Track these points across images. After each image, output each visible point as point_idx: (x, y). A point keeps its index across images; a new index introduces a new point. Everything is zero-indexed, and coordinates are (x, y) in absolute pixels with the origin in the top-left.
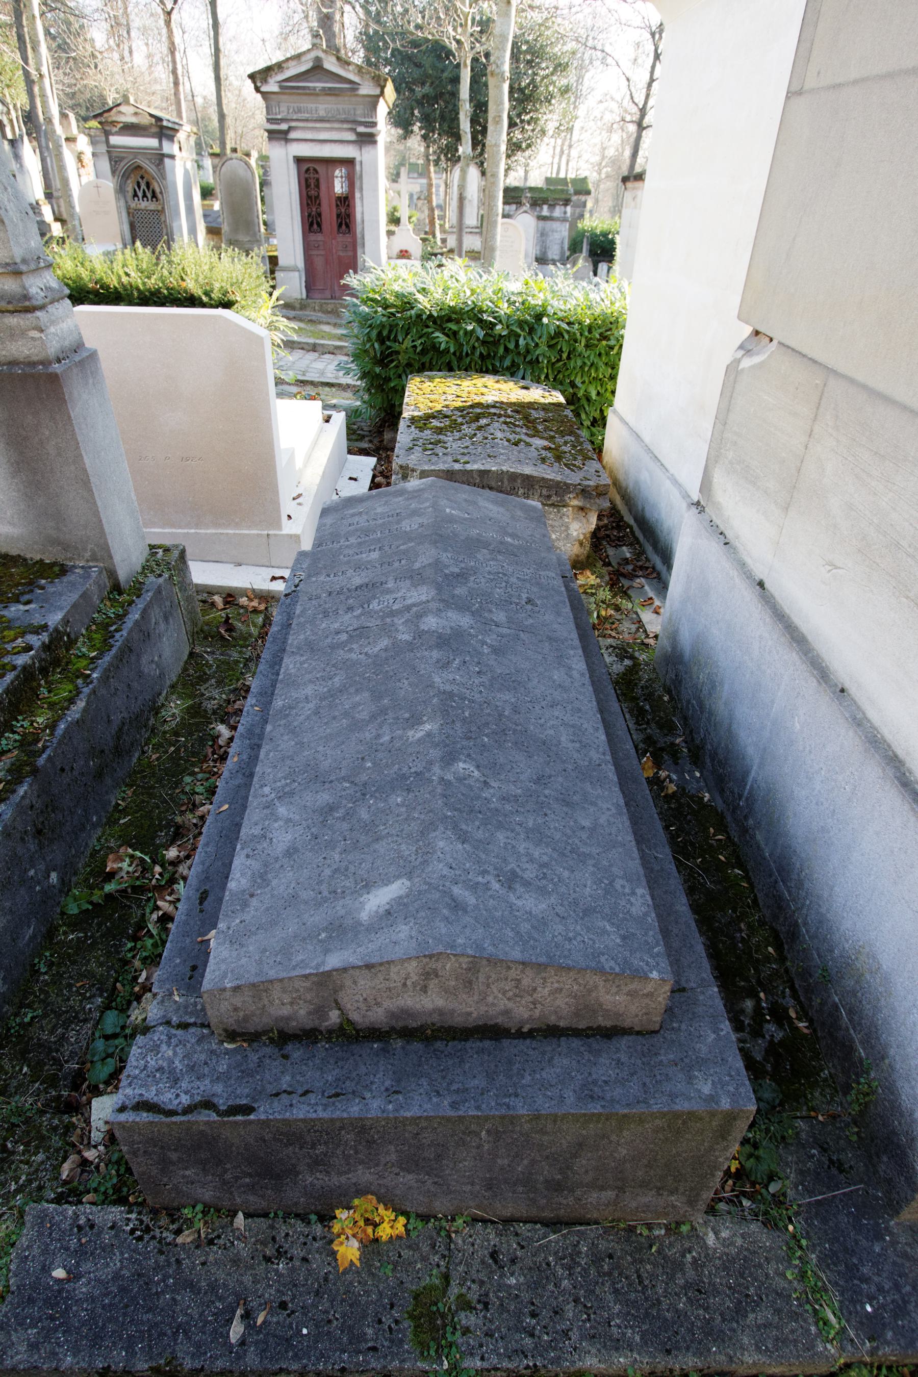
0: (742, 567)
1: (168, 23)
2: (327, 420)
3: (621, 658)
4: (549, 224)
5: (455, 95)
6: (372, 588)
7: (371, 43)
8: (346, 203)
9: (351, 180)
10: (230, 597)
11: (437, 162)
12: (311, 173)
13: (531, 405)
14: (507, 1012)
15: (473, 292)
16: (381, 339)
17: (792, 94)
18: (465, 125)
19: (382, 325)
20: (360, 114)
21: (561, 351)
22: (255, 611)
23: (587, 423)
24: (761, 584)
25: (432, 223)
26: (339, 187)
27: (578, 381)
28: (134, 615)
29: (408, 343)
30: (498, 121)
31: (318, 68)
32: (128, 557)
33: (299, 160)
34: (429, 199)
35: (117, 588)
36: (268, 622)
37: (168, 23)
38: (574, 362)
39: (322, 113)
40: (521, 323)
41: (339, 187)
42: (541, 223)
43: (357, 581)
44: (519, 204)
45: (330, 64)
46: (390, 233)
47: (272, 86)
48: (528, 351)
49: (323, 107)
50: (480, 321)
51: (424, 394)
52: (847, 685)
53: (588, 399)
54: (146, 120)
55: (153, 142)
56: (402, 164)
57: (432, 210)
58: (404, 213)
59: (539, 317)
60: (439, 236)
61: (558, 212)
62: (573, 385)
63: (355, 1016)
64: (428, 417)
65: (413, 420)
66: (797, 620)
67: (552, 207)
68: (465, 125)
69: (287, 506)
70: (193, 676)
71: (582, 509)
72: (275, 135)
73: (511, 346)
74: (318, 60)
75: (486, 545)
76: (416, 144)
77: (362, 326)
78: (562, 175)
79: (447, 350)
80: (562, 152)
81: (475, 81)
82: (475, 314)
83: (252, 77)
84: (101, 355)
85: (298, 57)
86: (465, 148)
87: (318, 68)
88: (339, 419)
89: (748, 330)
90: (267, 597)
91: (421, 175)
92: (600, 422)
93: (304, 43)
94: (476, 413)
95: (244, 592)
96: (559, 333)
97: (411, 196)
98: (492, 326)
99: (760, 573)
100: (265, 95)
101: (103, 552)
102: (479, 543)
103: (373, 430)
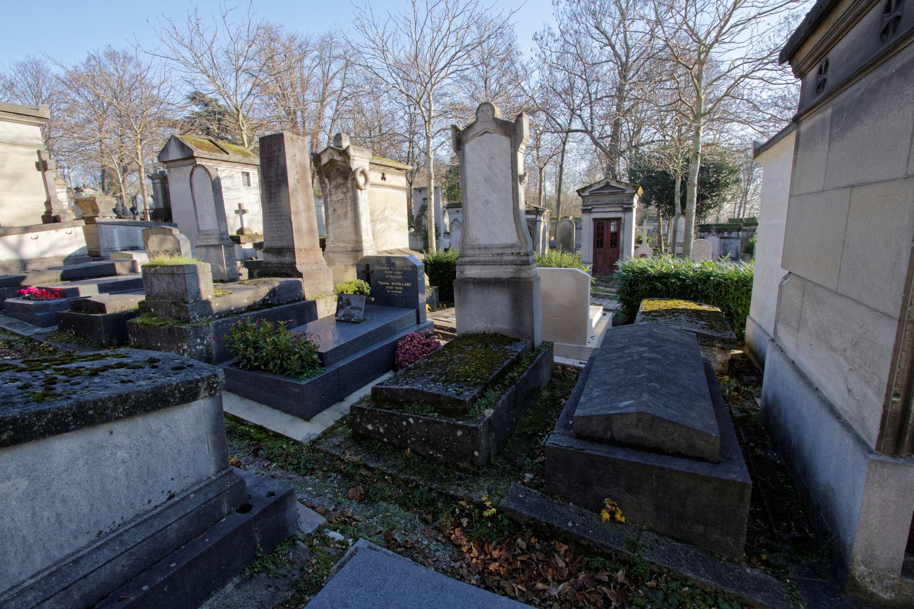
0: (787, 358)
1: (540, 173)
2: (604, 315)
3: (742, 412)
4: (728, 240)
5: (674, 188)
6: (625, 348)
7: (632, 173)
8: (615, 237)
9: (619, 227)
10: (564, 367)
11: (663, 216)
12: (600, 226)
13: (701, 311)
14: (663, 442)
15: (675, 267)
16: (630, 285)
17: (791, 196)
18: (677, 201)
19: (631, 280)
20: (625, 200)
21: (721, 292)
22: (574, 373)
23: (737, 325)
24: (793, 362)
25: (660, 242)
26: (612, 229)
27: (731, 305)
28: (539, 357)
29: (643, 287)
30: (692, 200)
31: (607, 186)
32: (538, 342)
33: (595, 220)
34: (659, 232)
35: (533, 349)
36: (578, 376)
37: (540, 173)
38: (732, 297)
39: (607, 201)
40: (699, 280)
41: (612, 229)
42: (723, 240)
43: (620, 346)
44: (709, 232)
45: (613, 183)
46: (636, 248)
47: (587, 193)
48: (703, 291)
49: (608, 199)
50: (679, 279)
51: (647, 305)
52: (819, 387)
53: (738, 314)
54: (532, 209)
55: (534, 217)
56: (645, 217)
57: (660, 236)
58: (644, 238)
59: (709, 277)
60: (663, 248)
61: (734, 234)
62: (728, 307)
63: (615, 435)
64: (650, 312)
65: (643, 313)
66: (804, 370)
67: (730, 232)
68: (677, 201)
69: (589, 339)
70: (551, 386)
71: (723, 348)
72: (584, 211)
73: (694, 289)
74: (608, 182)
75: (670, 341)
76: (653, 209)
77: (622, 280)
78: (741, 217)
79: (661, 290)
80: (740, 206)
81: (682, 182)
82: (676, 275)
83: (578, 191)
84: (542, 280)
85: (599, 182)
86: (678, 210)
87: (607, 186)
88: (610, 315)
89: (787, 272)
90: (579, 369)
91: (655, 221)
92: (743, 325)
93: (599, 176)
94: (673, 312)
95: (569, 366)
96: (719, 283)
97: (649, 231)
98: (684, 280)
99: (792, 357)
100: (582, 197)
101: (532, 337)
102: (667, 340)
103: (626, 315)
